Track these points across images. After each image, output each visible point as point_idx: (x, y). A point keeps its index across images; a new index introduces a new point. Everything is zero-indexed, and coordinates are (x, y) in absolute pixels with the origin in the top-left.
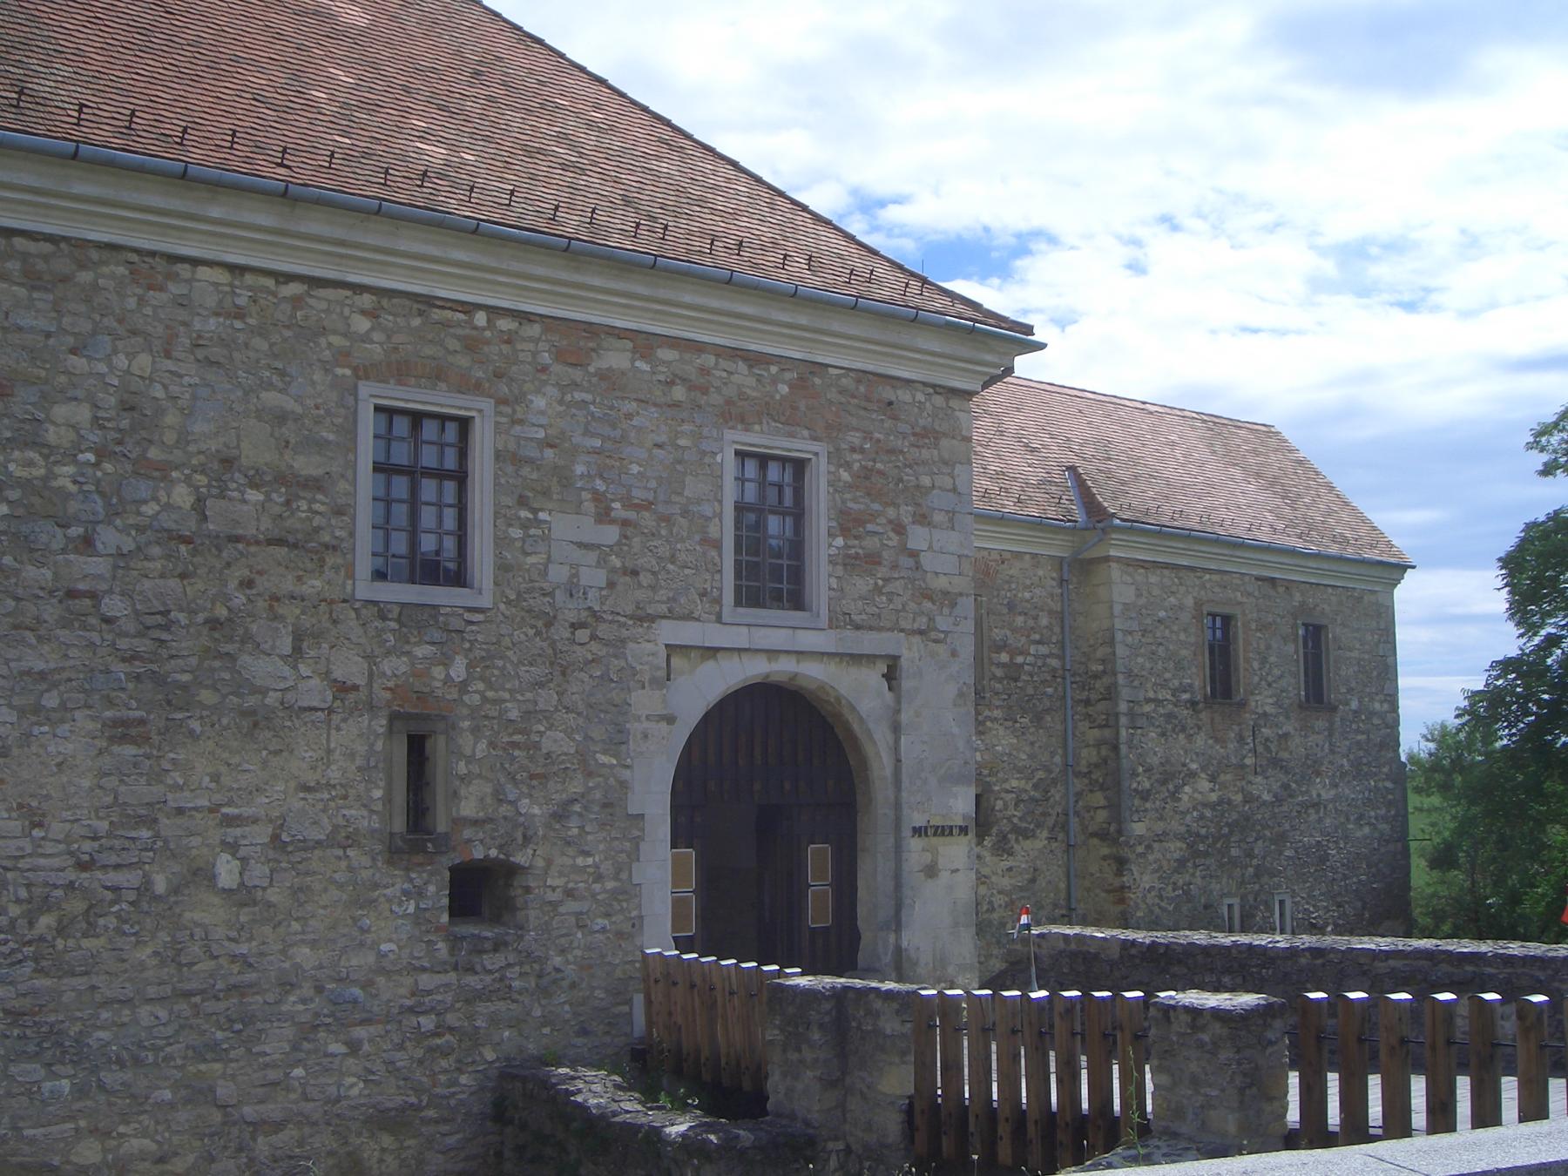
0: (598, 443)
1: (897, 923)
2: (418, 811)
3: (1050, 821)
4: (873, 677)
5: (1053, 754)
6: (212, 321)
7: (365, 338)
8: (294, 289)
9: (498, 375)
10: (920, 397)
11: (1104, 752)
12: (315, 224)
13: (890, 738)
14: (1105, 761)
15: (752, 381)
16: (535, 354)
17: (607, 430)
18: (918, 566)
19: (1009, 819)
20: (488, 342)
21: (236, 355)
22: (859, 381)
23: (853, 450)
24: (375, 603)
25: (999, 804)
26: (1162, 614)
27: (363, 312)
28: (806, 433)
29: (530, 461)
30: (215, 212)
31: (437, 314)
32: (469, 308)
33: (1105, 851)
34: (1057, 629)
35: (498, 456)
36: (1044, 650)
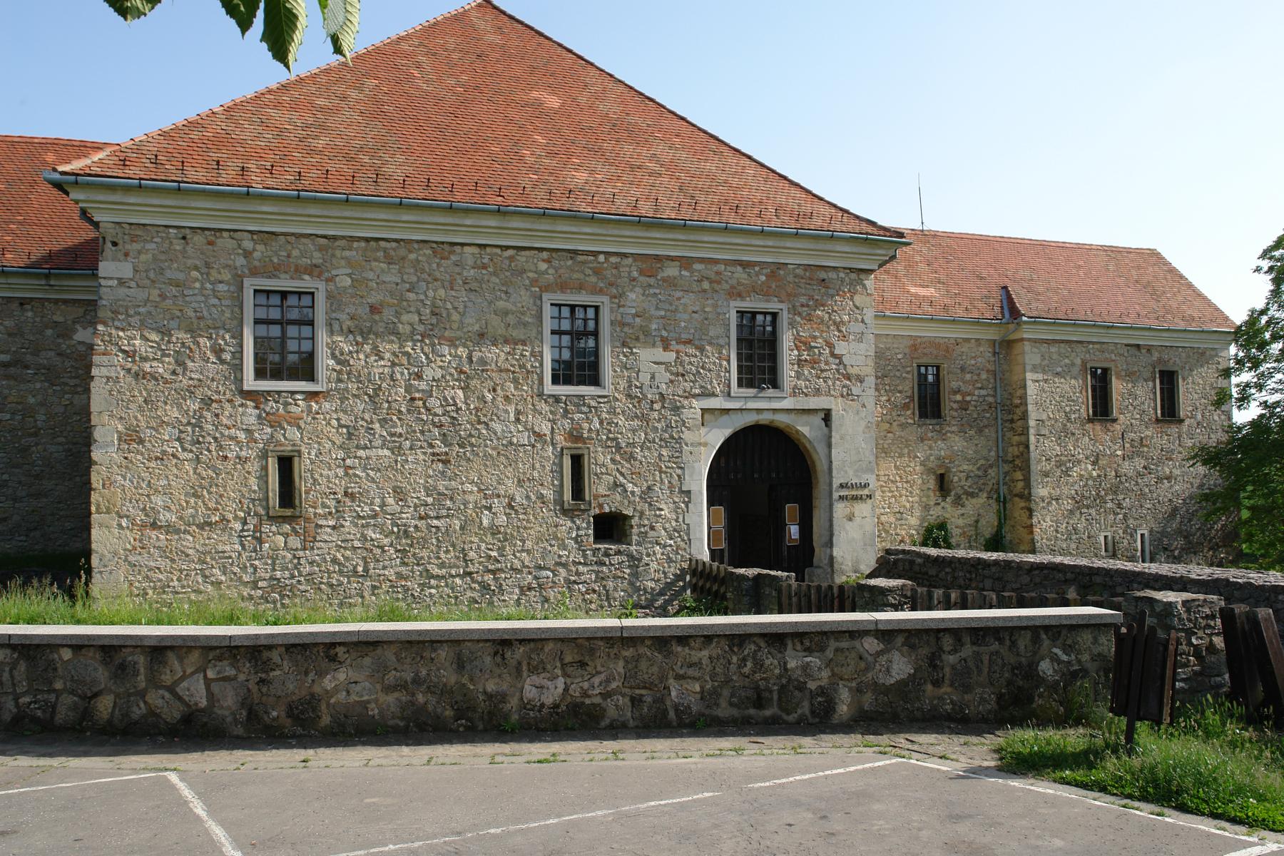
0: (663, 313)
1: (830, 544)
2: (578, 492)
3: (988, 488)
4: (817, 420)
5: (990, 451)
6: (472, 271)
7: (546, 272)
8: (511, 252)
9: (611, 284)
10: (842, 275)
11: (1021, 449)
12: (516, 223)
13: (826, 450)
14: (1022, 454)
15: (745, 276)
16: (629, 273)
17: (667, 307)
18: (841, 362)
19: (962, 487)
20: (606, 269)
21: (484, 286)
22: (806, 270)
23: (802, 306)
24: (554, 396)
25: (956, 479)
26: (1059, 369)
27: (544, 261)
28: (776, 299)
29: (629, 324)
30: (468, 222)
31: (581, 258)
32: (595, 254)
33: (1023, 504)
34: (992, 381)
35: (612, 323)
36: (983, 392)
